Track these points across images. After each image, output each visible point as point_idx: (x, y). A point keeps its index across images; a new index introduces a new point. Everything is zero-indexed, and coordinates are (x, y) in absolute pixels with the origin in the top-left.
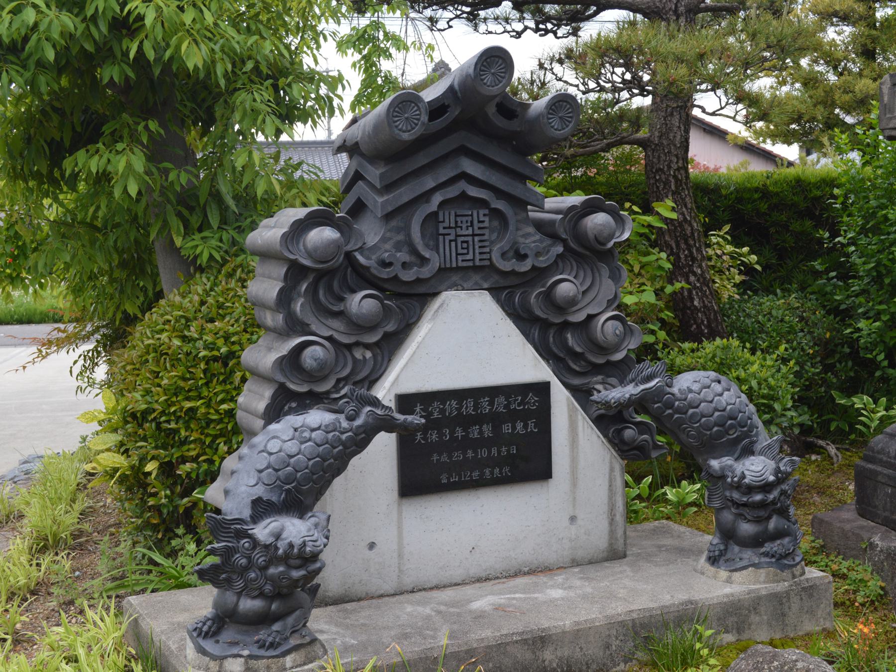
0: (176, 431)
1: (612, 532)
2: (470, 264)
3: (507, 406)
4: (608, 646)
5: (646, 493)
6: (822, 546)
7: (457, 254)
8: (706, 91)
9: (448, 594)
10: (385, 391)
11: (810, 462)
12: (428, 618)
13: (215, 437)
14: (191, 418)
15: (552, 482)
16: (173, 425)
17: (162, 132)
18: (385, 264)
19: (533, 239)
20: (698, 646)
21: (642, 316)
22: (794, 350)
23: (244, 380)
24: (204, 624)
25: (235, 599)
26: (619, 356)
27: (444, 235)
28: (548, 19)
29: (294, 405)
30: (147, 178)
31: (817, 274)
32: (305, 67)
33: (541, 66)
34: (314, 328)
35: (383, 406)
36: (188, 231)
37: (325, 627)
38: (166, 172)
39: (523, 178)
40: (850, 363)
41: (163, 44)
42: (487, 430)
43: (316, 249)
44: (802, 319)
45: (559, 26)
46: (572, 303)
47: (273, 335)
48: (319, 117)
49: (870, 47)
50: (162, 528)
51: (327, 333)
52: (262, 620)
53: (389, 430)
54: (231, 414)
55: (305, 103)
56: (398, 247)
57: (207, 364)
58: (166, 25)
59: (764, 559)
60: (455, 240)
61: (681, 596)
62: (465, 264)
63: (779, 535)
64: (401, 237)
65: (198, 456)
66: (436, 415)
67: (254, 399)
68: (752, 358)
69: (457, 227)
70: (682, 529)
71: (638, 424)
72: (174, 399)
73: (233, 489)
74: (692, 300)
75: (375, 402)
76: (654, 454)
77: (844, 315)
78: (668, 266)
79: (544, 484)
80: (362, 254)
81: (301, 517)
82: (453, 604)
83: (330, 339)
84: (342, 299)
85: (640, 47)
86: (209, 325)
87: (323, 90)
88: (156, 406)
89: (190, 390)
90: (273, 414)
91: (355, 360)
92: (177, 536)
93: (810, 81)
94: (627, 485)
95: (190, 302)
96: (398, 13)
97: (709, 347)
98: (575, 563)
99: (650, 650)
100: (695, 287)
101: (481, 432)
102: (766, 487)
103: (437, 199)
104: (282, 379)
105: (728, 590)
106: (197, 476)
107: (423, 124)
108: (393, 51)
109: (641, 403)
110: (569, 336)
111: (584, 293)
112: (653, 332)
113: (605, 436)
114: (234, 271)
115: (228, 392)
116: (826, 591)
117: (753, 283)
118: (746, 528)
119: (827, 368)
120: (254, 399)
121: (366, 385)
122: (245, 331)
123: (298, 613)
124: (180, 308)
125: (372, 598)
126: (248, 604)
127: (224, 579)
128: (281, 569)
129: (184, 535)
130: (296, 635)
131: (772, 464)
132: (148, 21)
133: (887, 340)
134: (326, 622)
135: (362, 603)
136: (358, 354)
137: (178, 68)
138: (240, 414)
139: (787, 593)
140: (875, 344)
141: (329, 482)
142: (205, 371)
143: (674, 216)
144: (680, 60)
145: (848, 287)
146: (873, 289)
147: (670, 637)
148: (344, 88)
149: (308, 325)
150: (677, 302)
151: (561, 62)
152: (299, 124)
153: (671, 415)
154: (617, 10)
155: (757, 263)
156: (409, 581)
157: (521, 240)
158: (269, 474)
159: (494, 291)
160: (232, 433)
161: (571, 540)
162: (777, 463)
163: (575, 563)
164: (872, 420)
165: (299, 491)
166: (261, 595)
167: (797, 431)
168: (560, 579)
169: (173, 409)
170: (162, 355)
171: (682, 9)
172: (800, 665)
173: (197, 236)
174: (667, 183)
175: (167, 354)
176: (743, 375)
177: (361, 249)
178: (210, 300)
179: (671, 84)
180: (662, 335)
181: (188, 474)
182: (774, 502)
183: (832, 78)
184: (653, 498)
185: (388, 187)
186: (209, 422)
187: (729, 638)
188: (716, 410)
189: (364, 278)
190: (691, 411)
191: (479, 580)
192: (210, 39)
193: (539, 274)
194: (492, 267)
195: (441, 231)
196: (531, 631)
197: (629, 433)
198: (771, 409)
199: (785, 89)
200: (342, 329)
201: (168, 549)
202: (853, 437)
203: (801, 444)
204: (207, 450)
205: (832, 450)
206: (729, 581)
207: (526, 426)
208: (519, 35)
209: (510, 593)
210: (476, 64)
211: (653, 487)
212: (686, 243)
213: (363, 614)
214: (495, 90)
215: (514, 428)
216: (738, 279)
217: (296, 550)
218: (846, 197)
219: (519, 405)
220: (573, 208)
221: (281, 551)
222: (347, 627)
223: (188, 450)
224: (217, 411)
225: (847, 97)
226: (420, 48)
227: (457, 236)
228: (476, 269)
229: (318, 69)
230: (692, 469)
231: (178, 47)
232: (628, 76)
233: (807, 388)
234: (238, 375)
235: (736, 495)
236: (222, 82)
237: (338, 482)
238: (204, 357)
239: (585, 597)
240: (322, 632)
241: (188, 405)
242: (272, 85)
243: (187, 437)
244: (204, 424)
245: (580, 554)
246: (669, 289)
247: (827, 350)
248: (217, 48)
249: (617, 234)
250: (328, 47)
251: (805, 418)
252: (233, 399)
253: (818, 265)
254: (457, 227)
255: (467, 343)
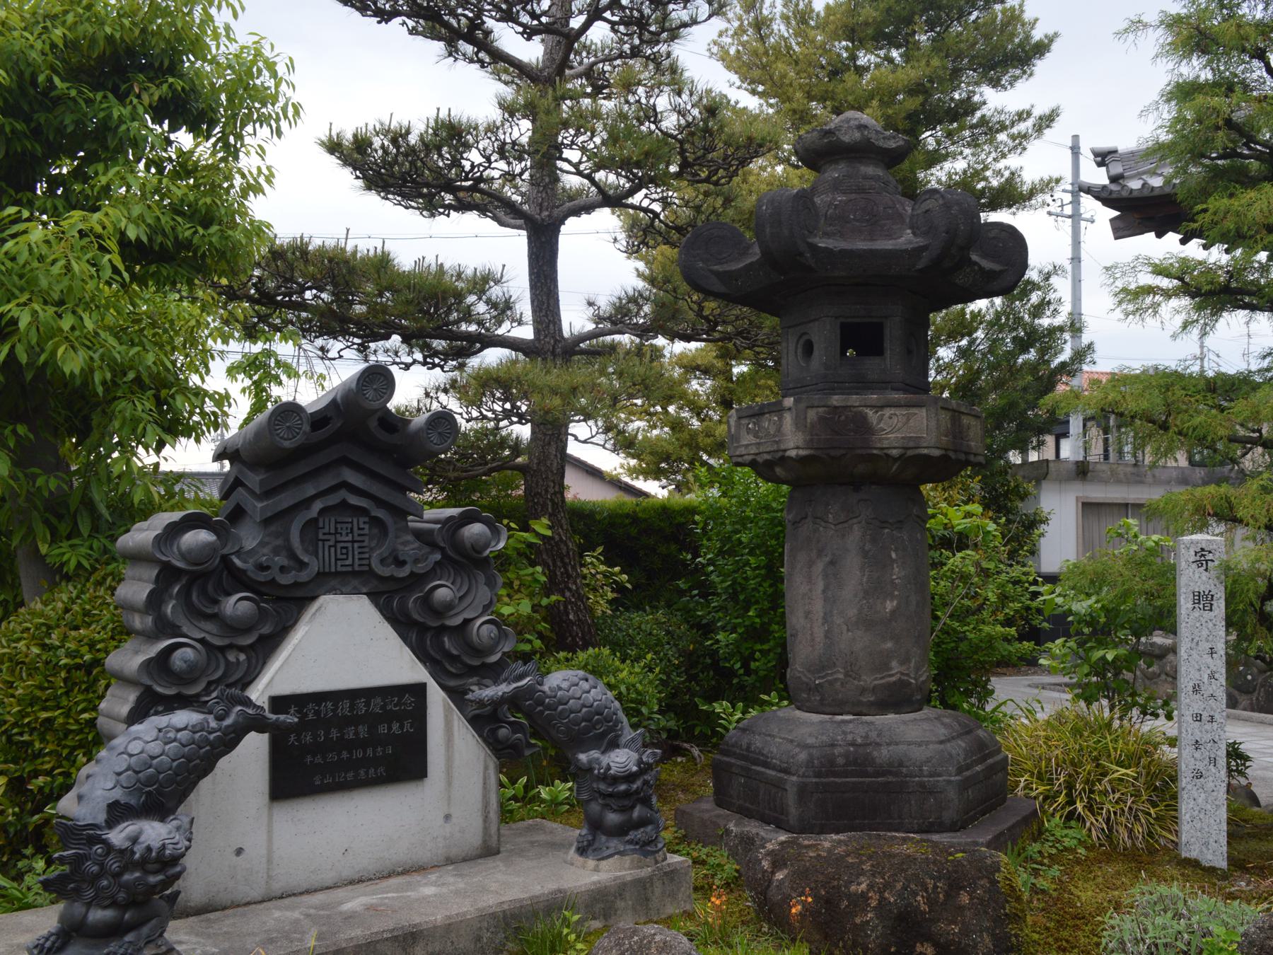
0: (30, 743)
1: (486, 829)
2: (350, 569)
3: (383, 708)
4: (478, 939)
5: (521, 793)
6: (685, 836)
7: (336, 560)
8: (579, 421)
9: (319, 898)
10: (259, 693)
11: (676, 764)
12: (297, 921)
13: (74, 749)
14: (47, 730)
15: (427, 781)
16: (26, 737)
17: (32, 436)
18: (262, 568)
19: (412, 546)
20: (565, 931)
21: (520, 627)
22: (661, 660)
23: (107, 686)
24: (47, 939)
25: (84, 910)
26: (494, 658)
27: (324, 540)
28: (436, 353)
29: (160, 709)
30: (12, 482)
31: (682, 593)
32: (191, 384)
33: (427, 395)
34: (185, 630)
35: (255, 706)
36: (55, 539)
37: (184, 938)
38: (34, 477)
39: (403, 489)
40: (711, 673)
41: (37, 349)
42: (363, 731)
43: (190, 551)
44: (668, 632)
45: (446, 361)
46: (449, 607)
47: (141, 638)
48: (203, 433)
49: (728, 397)
50: (8, 850)
51: (200, 635)
52: (112, 931)
53: (261, 730)
54: (92, 723)
55: (190, 418)
56: (276, 551)
57: (68, 672)
58: (41, 329)
59: (628, 847)
60: (335, 546)
61: (551, 886)
62: (344, 569)
63: (643, 823)
64: (279, 542)
65: (53, 769)
66: (311, 716)
67: (118, 702)
68: (622, 666)
69: (336, 533)
70: (555, 825)
71: (510, 723)
72: (29, 710)
73: (91, 794)
74: (568, 615)
75: (248, 702)
76: (528, 753)
77: (707, 629)
78: (543, 579)
79: (419, 783)
80: (238, 558)
81: (162, 819)
82: (322, 907)
83: (202, 641)
84: (216, 602)
85: (518, 378)
86: (73, 633)
87: (209, 406)
88: (8, 718)
89: (46, 700)
90: (137, 715)
91: (227, 662)
92: (25, 857)
93: (677, 426)
94: (501, 785)
95: (53, 609)
96: (291, 342)
97: (582, 656)
98: (450, 861)
99: (520, 940)
100: (571, 602)
101: (356, 733)
102: (629, 778)
103: (318, 506)
104: (149, 682)
105: (595, 878)
106: (51, 790)
107: (305, 433)
108: (284, 378)
109: (513, 701)
110: (446, 639)
111: (461, 598)
112: (530, 641)
113: (480, 736)
114: (104, 579)
115: (90, 701)
116: (686, 874)
117: (624, 600)
118: (613, 818)
119: (692, 678)
120: (118, 702)
121: (240, 686)
122: (113, 638)
123: (154, 922)
124: (42, 615)
125: (238, 906)
126: (98, 915)
127: (73, 889)
128: (137, 874)
129: (33, 855)
130: (151, 945)
131: (635, 756)
132: (23, 324)
133: (743, 651)
134: (186, 933)
135: (227, 912)
136: (231, 657)
137: (52, 374)
138: (101, 721)
139: (651, 878)
140: (732, 655)
141: (194, 784)
142: (65, 680)
143: (549, 533)
144: (554, 391)
145: (709, 602)
146: (730, 605)
147: (540, 927)
148: (230, 406)
149: (179, 627)
150: (553, 614)
151: (446, 391)
152: (182, 439)
153: (542, 712)
154: (499, 349)
155: (628, 581)
156: (277, 887)
157: (400, 547)
158: (129, 776)
159: (373, 596)
160: (93, 740)
161: (445, 838)
162: (641, 755)
163: (450, 861)
164: (730, 723)
165: (163, 791)
166: (114, 904)
167: (664, 736)
168: (433, 877)
169: (26, 721)
170: (18, 663)
171: (558, 350)
172: (658, 938)
173: (65, 544)
174: (544, 506)
175: (23, 663)
176: (613, 681)
177: (238, 553)
178: (76, 608)
179: (547, 413)
180: (538, 643)
181: (41, 789)
182: (637, 792)
183: (696, 423)
184: (528, 798)
185: (268, 494)
186: (67, 733)
187: (596, 924)
188: (584, 706)
189: (240, 581)
190: (561, 707)
191: (352, 882)
192: (89, 348)
193: (417, 580)
194: (371, 572)
195: (321, 536)
196: (402, 928)
197: (503, 732)
198: (639, 713)
199: (656, 432)
200: (215, 631)
201: (13, 873)
202: (714, 740)
203: (671, 747)
204: (64, 763)
205: (696, 752)
206: (596, 869)
207: (402, 727)
208: (407, 367)
209: (383, 893)
210: (359, 379)
211: (527, 788)
212: (562, 561)
213: (227, 922)
214: (376, 405)
215: (390, 728)
216: (610, 595)
217: (154, 854)
218: (706, 524)
219: (396, 705)
220: (451, 518)
221: (137, 856)
222: (209, 936)
223: (42, 764)
224: (77, 721)
225: (709, 440)
226: (312, 377)
227: (337, 542)
228: (354, 574)
229: (205, 387)
230: (566, 769)
231: (54, 353)
232: (508, 406)
233: (674, 696)
234: (103, 683)
235: (602, 787)
236: (100, 390)
237: (205, 784)
238: (66, 665)
239: (457, 893)
240: (180, 943)
241: (44, 715)
242: (154, 395)
243: (41, 750)
244: (61, 734)
245: (454, 852)
246: (545, 602)
247: (691, 661)
248: (96, 356)
249: (493, 544)
250: (218, 367)
251: (672, 724)
252: (95, 708)
253: (682, 584)
254: (336, 533)
255: (342, 646)
